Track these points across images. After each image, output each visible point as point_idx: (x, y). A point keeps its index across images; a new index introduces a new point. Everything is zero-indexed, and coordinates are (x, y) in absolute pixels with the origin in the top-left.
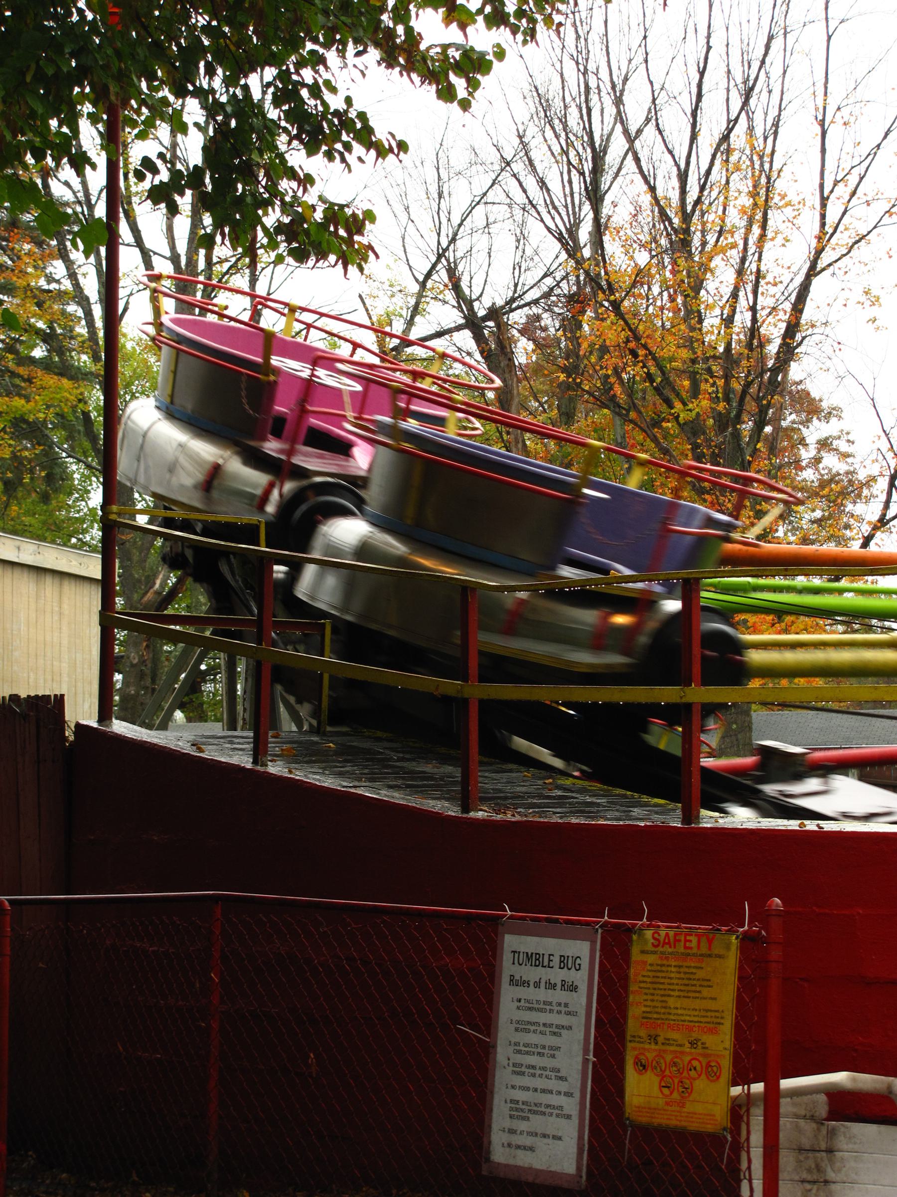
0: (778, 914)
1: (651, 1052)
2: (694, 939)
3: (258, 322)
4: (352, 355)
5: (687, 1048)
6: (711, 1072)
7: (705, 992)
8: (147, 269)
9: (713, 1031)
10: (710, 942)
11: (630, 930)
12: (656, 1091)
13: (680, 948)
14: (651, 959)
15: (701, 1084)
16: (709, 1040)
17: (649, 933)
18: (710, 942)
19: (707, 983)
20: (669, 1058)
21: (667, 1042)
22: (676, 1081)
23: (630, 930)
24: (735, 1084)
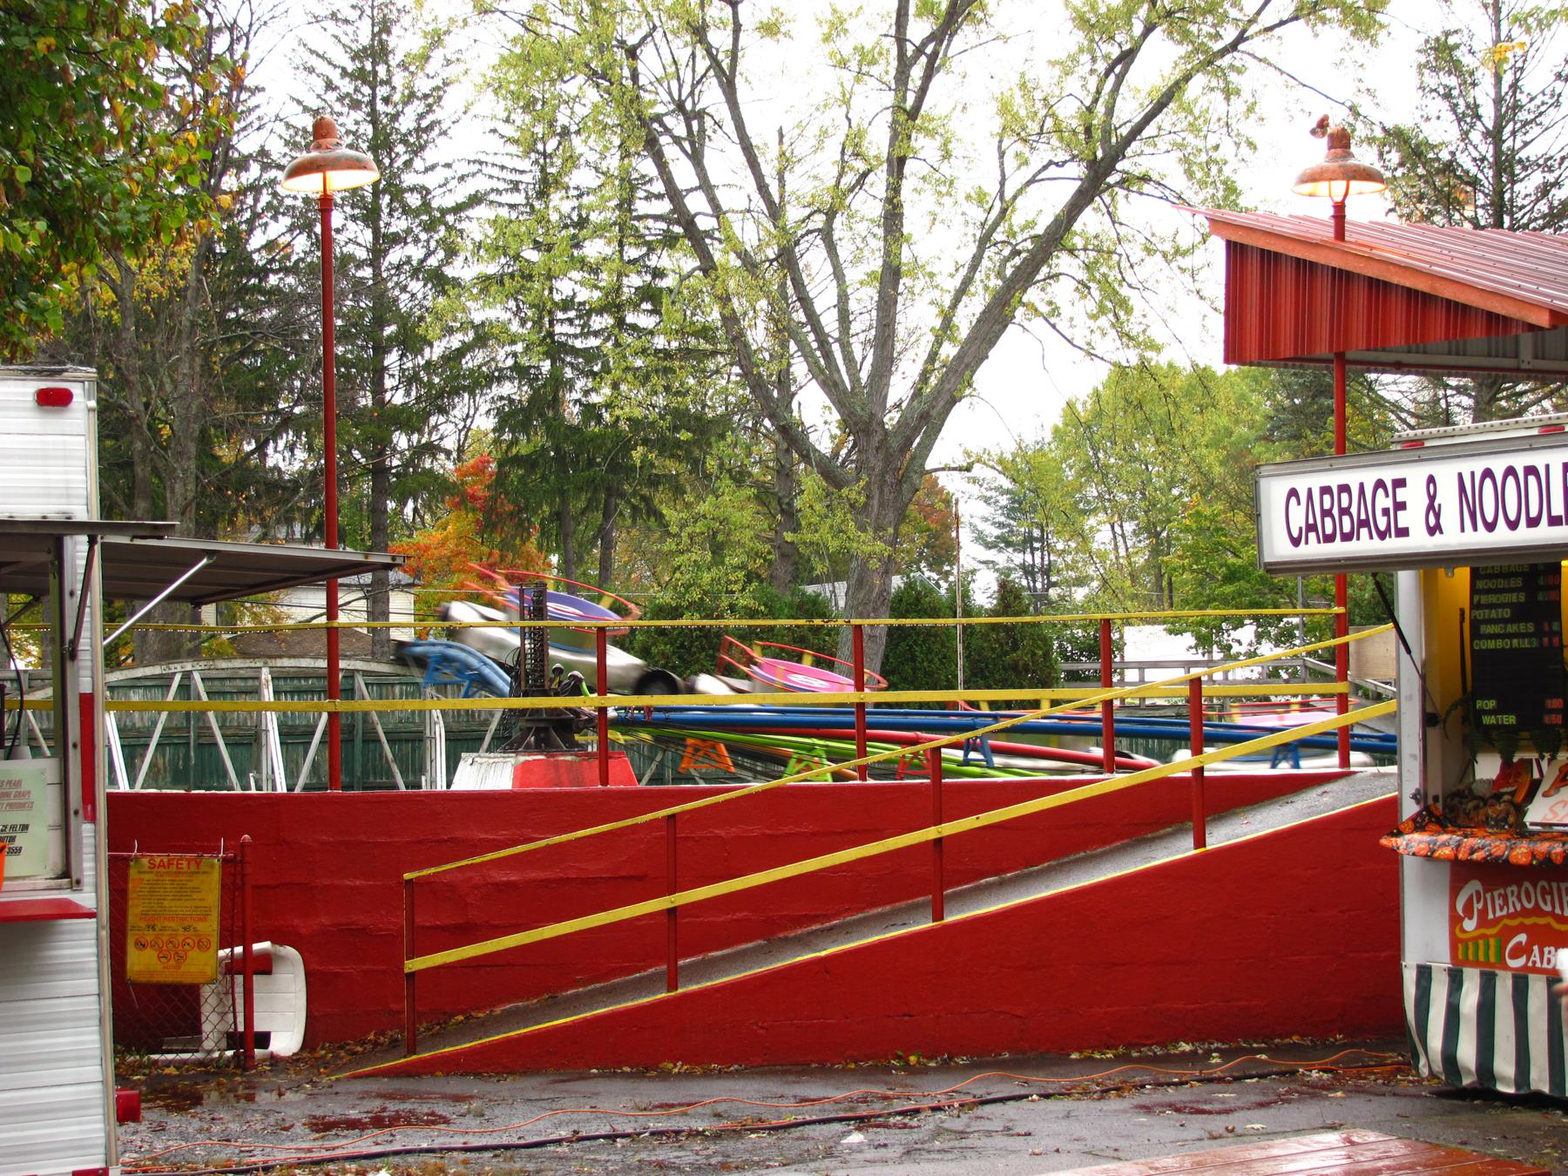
0: (249, 845)
1: (149, 936)
2: (185, 864)
3: (1482, 974)
4: (448, 786)
5: (181, 931)
6: (202, 945)
7: (195, 896)
8: (1494, 975)
9: (203, 918)
10: (198, 864)
11: (127, 860)
12: (155, 959)
13: (173, 869)
14: (147, 876)
15: (194, 954)
16: (200, 926)
17: (145, 861)
18: (198, 864)
19: (197, 890)
20: (165, 939)
21: (163, 929)
22: (173, 952)
23: (127, 860)
24: (222, 947)
